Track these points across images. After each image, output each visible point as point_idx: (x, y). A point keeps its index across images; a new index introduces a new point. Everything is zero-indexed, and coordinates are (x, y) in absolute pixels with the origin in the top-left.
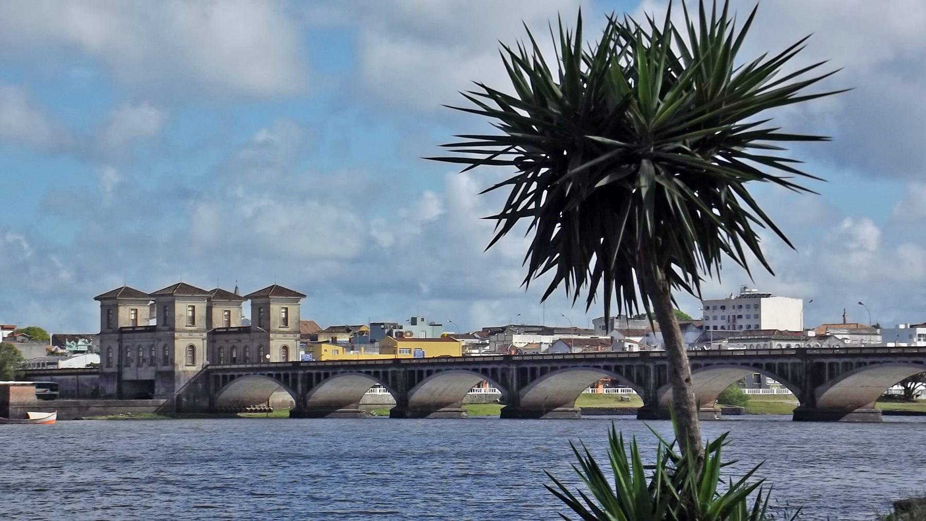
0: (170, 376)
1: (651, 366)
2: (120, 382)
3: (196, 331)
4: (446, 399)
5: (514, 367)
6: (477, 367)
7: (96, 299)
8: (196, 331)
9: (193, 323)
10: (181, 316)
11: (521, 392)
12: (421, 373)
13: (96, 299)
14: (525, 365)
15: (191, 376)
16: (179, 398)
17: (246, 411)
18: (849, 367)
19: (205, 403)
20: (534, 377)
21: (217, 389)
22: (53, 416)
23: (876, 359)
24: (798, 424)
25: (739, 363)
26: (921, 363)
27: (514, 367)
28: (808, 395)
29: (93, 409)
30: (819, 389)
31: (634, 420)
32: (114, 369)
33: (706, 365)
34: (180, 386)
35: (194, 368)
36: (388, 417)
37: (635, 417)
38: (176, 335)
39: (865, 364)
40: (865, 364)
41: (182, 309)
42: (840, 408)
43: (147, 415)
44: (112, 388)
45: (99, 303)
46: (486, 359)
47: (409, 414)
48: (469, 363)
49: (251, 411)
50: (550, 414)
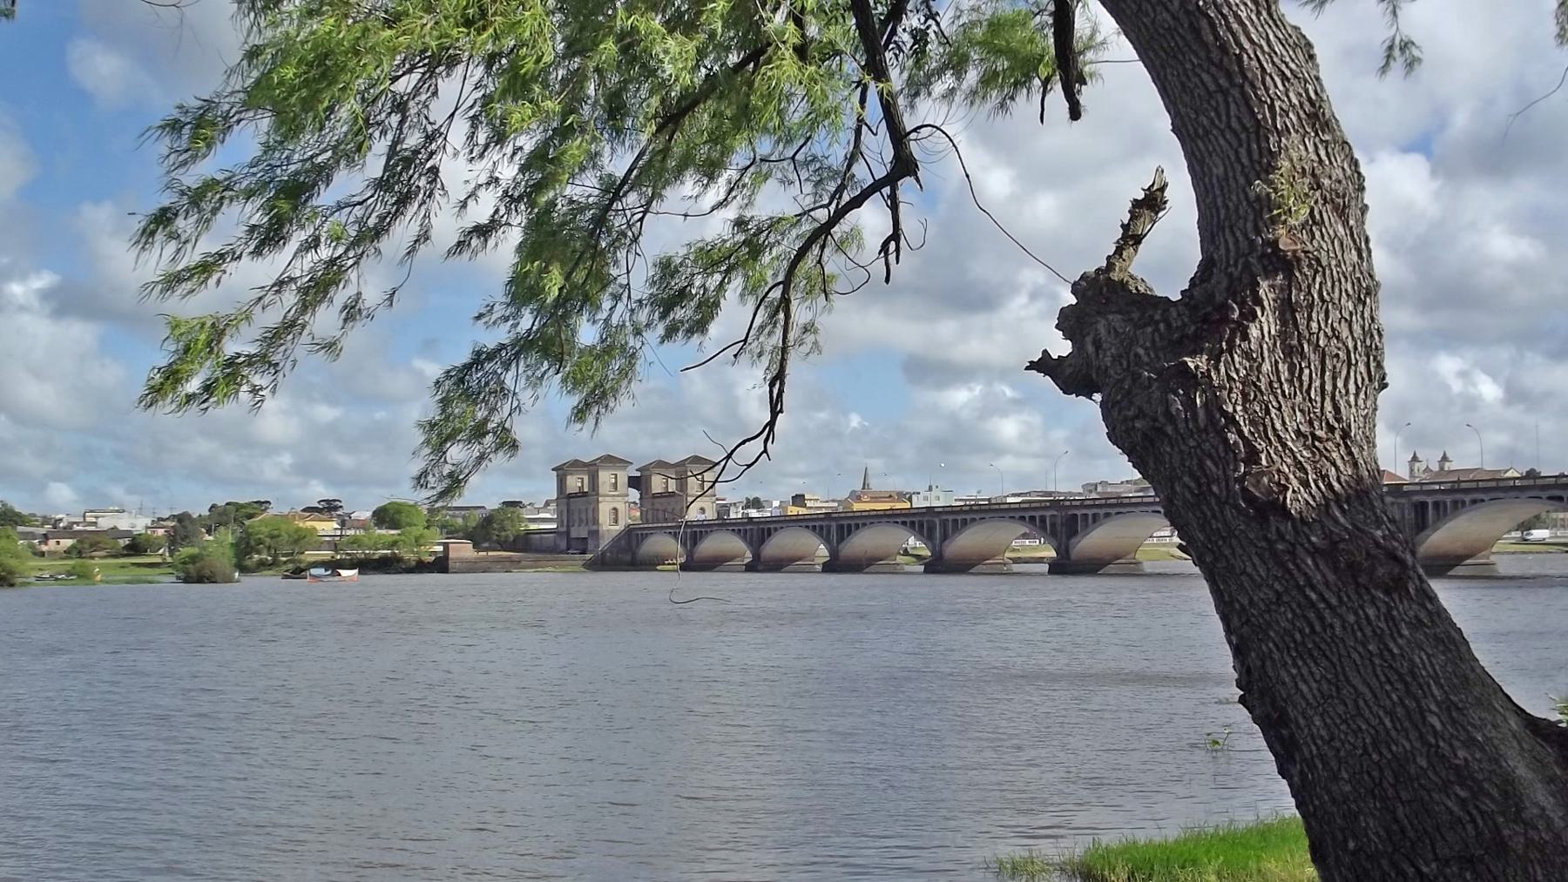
0: (595, 534)
1: (937, 521)
2: (569, 539)
3: (618, 496)
4: (799, 554)
5: (834, 524)
6: (1022, 514)
7: (553, 470)
8: (618, 496)
9: (616, 489)
10: (604, 482)
11: (840, 547)
12: (769, 529)
13: (553, 470)
14: (842, 522)
15: (615, 534)
16: (603, 553)
17: (664, 564)
18: (1460, 505)
19: (628, 558)
20: (849, 533)
21: (638, 545)
22: (355, 572)
23: (1122, 510)
24: (1058, 579)
25: (1544, 497)
26: (1560, 499)
27: (834, 524)
28: (1063, 547)
29: (523, 563)
30: (1073, 541)
31: (1042, 574)
32: (564, 529)
33: (1474, 502)
34: (604, 543)
35: (617, 528)
36: (1045, 568)
37: (922, 568)
38: (600, 499)
39: (1483, 501)
40: (1483, 501)
41: (605, 477)
42: (1100, 559)
43: (576, 569)
44: (563, 545)
45: (555, 473)
46: (1133, 500)
47: (760, 568)
48: (1544, 488)
49: (669, 564)
50: (872, 568)
